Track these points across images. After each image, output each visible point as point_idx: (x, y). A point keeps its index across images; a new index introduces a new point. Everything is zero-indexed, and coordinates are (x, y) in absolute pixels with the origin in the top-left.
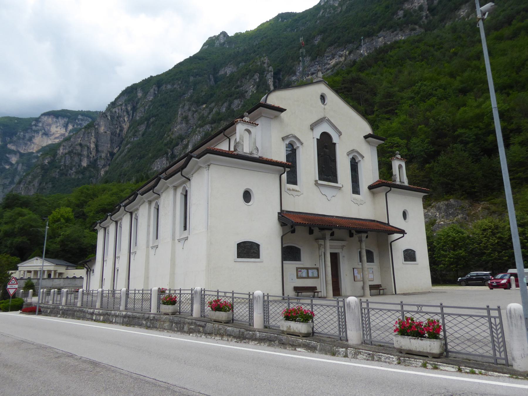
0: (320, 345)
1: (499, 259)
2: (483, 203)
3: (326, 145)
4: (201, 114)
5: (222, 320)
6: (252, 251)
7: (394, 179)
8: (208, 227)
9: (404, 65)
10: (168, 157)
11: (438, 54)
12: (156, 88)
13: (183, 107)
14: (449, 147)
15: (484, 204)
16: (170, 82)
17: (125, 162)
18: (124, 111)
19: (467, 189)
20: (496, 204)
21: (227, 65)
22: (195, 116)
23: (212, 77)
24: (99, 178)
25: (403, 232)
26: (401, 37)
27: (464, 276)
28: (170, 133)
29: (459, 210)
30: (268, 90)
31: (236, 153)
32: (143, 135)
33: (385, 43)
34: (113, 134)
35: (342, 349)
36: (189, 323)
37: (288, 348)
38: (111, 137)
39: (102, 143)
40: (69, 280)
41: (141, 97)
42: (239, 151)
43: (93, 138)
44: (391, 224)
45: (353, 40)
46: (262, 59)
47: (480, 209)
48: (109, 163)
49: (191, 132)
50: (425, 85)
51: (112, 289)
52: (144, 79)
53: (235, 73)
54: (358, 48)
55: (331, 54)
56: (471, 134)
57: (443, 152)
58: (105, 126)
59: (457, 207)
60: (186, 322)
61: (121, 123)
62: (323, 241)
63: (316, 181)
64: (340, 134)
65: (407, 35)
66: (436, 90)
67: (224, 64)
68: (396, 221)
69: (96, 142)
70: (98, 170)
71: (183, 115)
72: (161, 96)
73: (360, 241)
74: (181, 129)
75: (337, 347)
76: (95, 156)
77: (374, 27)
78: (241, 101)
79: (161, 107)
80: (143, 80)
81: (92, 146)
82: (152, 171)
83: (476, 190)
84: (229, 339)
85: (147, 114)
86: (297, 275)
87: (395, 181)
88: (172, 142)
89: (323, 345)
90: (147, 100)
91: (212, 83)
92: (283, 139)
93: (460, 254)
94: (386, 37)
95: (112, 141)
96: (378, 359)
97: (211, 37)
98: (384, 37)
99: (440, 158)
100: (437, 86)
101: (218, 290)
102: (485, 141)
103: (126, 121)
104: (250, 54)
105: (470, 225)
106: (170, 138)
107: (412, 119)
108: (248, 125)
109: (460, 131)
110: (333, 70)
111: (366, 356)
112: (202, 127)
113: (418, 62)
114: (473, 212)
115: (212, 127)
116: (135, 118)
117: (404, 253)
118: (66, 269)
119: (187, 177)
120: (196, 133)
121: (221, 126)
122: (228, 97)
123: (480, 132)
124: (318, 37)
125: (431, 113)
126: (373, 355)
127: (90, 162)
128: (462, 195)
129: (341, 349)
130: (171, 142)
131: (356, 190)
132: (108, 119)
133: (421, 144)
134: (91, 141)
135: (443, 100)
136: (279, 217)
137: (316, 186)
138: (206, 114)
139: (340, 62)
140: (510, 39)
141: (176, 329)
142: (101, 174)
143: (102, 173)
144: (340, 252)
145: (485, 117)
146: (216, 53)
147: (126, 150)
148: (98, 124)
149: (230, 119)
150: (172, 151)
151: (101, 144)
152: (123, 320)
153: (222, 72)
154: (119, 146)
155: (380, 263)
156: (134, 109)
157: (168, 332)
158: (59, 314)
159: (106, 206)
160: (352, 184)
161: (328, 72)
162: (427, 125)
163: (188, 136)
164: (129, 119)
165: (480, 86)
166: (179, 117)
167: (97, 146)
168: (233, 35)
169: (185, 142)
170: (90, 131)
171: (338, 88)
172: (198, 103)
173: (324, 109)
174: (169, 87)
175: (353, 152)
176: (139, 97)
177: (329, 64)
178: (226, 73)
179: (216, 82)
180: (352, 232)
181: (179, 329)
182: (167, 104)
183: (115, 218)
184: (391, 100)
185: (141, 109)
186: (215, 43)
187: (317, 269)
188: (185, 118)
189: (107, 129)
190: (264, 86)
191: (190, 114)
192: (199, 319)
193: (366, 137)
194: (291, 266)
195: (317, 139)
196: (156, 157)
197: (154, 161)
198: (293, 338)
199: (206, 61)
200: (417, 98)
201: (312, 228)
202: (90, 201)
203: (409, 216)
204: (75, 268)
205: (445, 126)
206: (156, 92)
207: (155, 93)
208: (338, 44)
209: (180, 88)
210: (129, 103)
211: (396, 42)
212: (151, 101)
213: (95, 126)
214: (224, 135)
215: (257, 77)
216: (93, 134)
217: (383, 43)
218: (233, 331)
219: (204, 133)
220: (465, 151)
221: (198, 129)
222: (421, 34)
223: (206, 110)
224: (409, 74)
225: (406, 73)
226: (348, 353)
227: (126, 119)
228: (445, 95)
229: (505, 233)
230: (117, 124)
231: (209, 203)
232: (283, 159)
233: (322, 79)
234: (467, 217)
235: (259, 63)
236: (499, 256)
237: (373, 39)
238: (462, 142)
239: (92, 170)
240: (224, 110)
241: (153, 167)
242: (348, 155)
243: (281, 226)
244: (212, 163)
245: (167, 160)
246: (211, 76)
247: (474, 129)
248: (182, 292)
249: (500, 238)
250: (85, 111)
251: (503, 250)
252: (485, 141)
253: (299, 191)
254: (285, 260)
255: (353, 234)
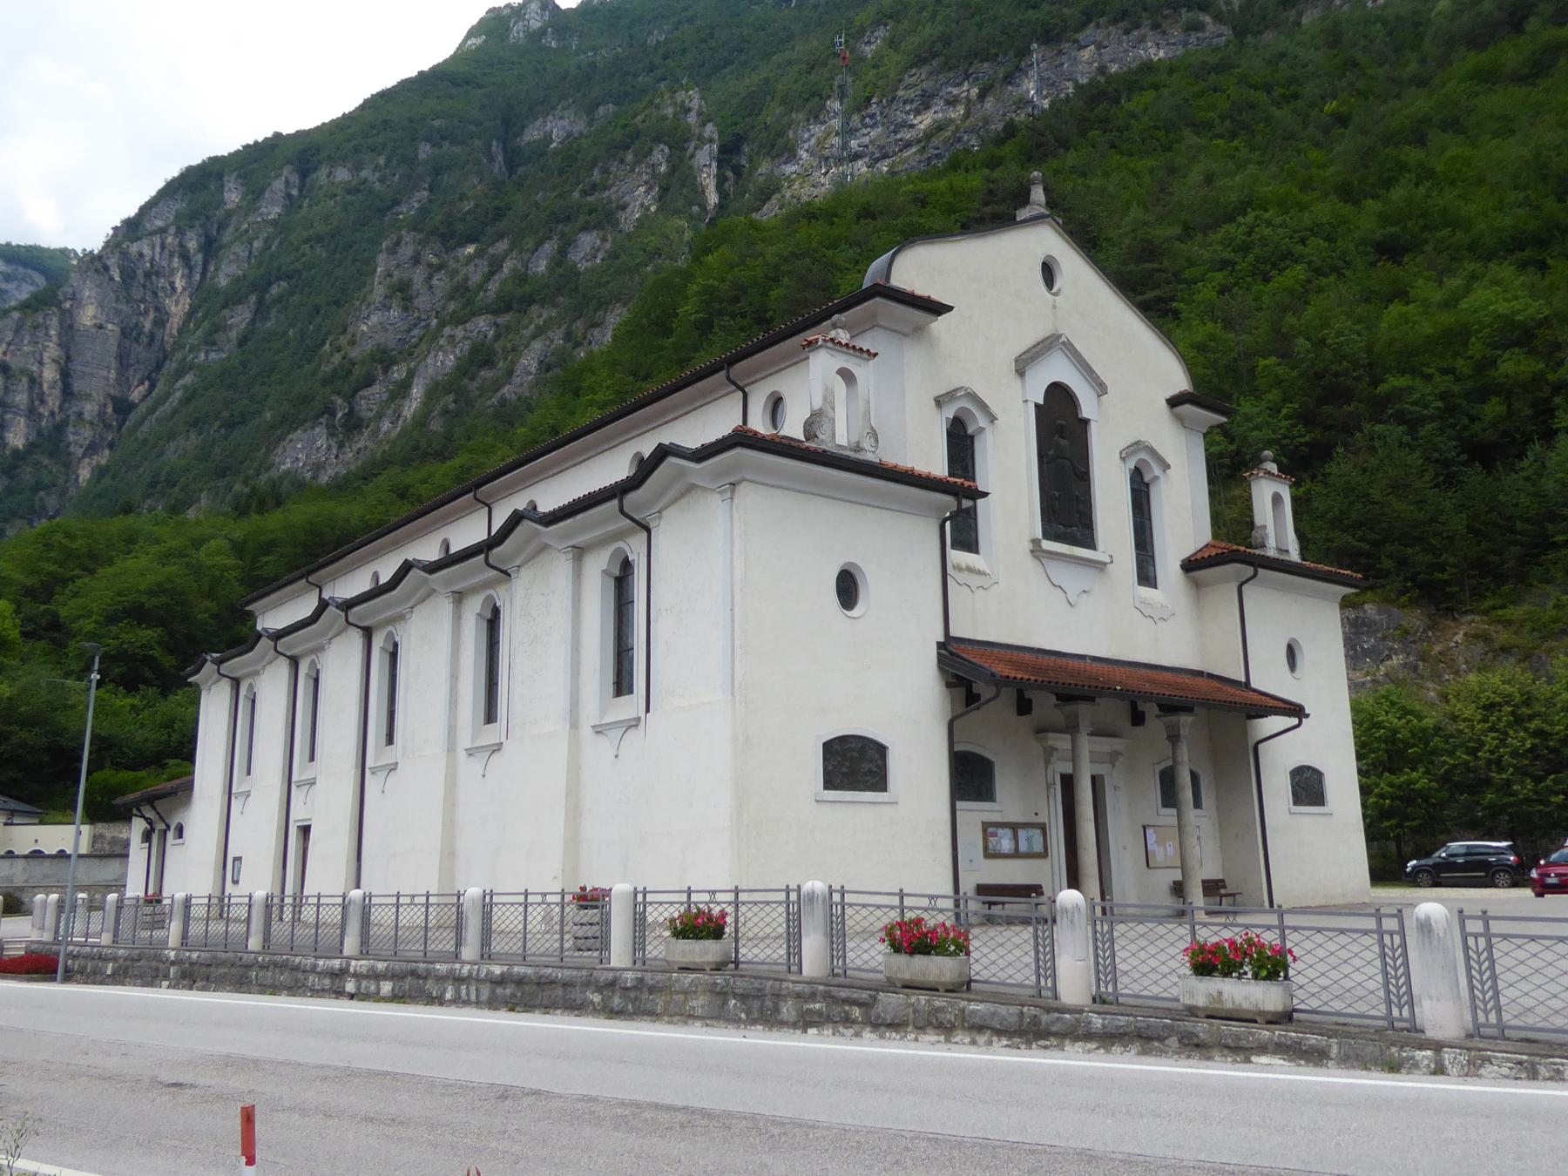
0: (1339, 1044)
1: (1540, 802)
2: (1469, 618)
3: (1062, 427)
4: (459, 278)
5: (939, 983)
6: (865, 766)
7: (1260, 540)
8: (733, 689)
9: (1175, 146)
10: (334, 426)
11: (1282, 114)
12: (295, 179)
13: (393, 251)
14: (1358, 434)
15: (1471, 622)
16: (344, 158)
17: (172, 436)
18: (171, 255)
19: (1419, 574)
20: (1509, 622)
21: (554, 108)
22: (435, 282)
23: (498, 147)
24: (72, 491)
25: (1297, 711)
26: (1156, 53)
27: (1429, 854)
28: (343, 340)
29: (1394, 640)
30: (699, 205)
31: (812, 445)
32: (243, 341)
33: (1102, 70)
34: (129, 333)
35: (1424, 1053)
36: (798, 996)
37: (1217, 1058)
38: (119, 344)
39: (86, 364)
40: (47, 863)
41: (239, 207)
42: (823, 441)
43: (51, 345)
44: (1253, 685)
45: (993, 51)
46: (681, 96)
47: (1459, 638)
48: (110, 438)
49: (421, 340)
50: (1269, 224)
51: (218, 894)
52: (251, 143)
53: (583, 140)
54: (1009, 79)
55: (918, 92)
56: (1429, 394)
57: (1340, 450)
58: (101, 305)
59: (1388, 628)
60: (784, 993)
61: (161, 294)
62: (1068, 737)
63: (1035, 542)
64: (1101, 389)
65: (1174, 44)
66: (1303, 241)
67: (542, 105)
68: (1270, 678)
69: (62, 361)
70: (68, 464)
71: (395, 279)
72: (310, 206)
73: (1174, 738)
74: (383, 326)
75: (1402, 1047)
76: (57, 410)
77: (1066, 11)
78: (604, 240)
79: (312, 247)
80: (247, 147)
81: (50, 374)
82: (274, 474)
83: (1446, 577)
84: (977, 1038)
85: (260, 265)
86: (986, 848)
87: (1263, 546)
88: (350, 372)
89: (1350, 1045)
90: (259, 219)
91: (496, 171)
92: (939, 402)
93: (1414, 784)
94: (1105, 47)
95: (123, 358)
96: (1552, 1073)
97: (494, 8)
98: (1100, 47)
99: (1331, 468)
100: (1306, 229)
101: (901, 890)
102: (1473, 419)
103: (179, 289)
104: (636, 76)
105: (1428, 689)
106: (344, 358)
107: (1231, 336)
108: (847, 357)
109: (1395, 382)
110: (924, 148)
111: (1511, 1069)
112: (462, 324)
113: (1220, 141)
114: (1437, 648)
115: (495, 324)
116: (212, 279)
117: (1292, 779)
118: (5, 824)
119: (637, 518)
120: (442, 342)
121: (531, 323)
122: (558, 222)
123: (1456, 388)
124: (876, 34)
125: (1299, 319)
126: (1533, 1065)
127: (39, 433)
128: (1401, 593)
129: (1419, 1054)
130: (348, 366)
131: (1146, 577)
132: (112, 279)
133: (1270, 420)
134: (46, 355)
135: (1325, 275)
136: (942, 660)
137: (1035, 557)
138: (476, 279)
139: (951, 120)
140: (1520, 79)
141: (743, 1016)
142: (78, 477)
143: (84, 473)
144: (1103, 773)
145: (1473, 340)
146: (513, 63)
147: (178, 394)
148: (74, 294)
149: (561, 299)
150: (349, 403)
151: (80, 368)
152: (493, 992)
153: (532, 134)
154: (149, 378)
155: (1218, 808)
156: (210, 247)
157: (707, 1025)
158: (166, 977)
159: (144, 599)
160: (1137, 554)
161: (909, 153)
162: (1285, 355)
163: (408, 352)
164: (189, 283)
165: (1440, 234)
166: (380, 283)
167: (65, 375)
168: (574, 6)
169: (399, 373)
170: (41, 320)
171: (972, 214)
172: (450, 237)
173: (1054, 307)
174: (342, 174)
175: (1139, 449)
176: (230, 206)
177: (912, 126)
178: (548, 138)
179: (511, 165)
180: (1140, 709)
181: (756, 1015)
182: (333, 236)
183: (289, 647)
184: (1156, 265)
185: (237, 250)
186: (508, 30)
187: (1043, 828)
188: (401, 290)
189: (108, 314)
190: (684, 191)
191: (418, 275)
192: (824, 981)
193: (1174, 402)
194: (974, 814)
195: (1037, 406)
196: (288, 423)
197: (281, 439)
198: (1236, 1028)
199: (480, 91)
200: (1243, 265)
201: (1028, 695)
202: (79, 577)
203: (1306, 658)
204: (37, 821)
205: (1345, 363)
206: (295, 192)
207: (289, 196)
208: (942, 59)
209: (382, 180)
210: (191, 227)
211: (1148, 67)
212: (274, 223)
213: (61, 302)
214: (728, 378)
215: (660, 155)
216: (53, 332)
217: (1096, 65)
218: (994, 1014)
219: (467, 345)
220: (1412, 449)
221: (447, 330)
222: (1226, 46)
223: (476, 265)
224: (1209, 179)
225: (1195, 176)
226: (1447, 1063)
227: (179, 284)
228: (1331, 257)
229: (1557, 718)
230: (143, 300)
231: (736, 608)
232: (937, 466)
233: (1043, 211)
234: (1420, 663)
235: (669, 111)
236: (1536, 792)
237: (1060, 53)
238: (1401, 418)
239: (46, 462)
240: (542, 266)
241: (277, 460)
242: (1123, 459)
243: (949, 685)
244: (748, 477)
245: (331, 435)
246: (494, 143)
247: (1437, 378)
248: (743, 897)
249: (1539, 733)
250: (19, 246)
251: (1549, 773)
252: (1473, 419)
253: (988, 571)
254: (962, 799)
255: (1142, 715)
